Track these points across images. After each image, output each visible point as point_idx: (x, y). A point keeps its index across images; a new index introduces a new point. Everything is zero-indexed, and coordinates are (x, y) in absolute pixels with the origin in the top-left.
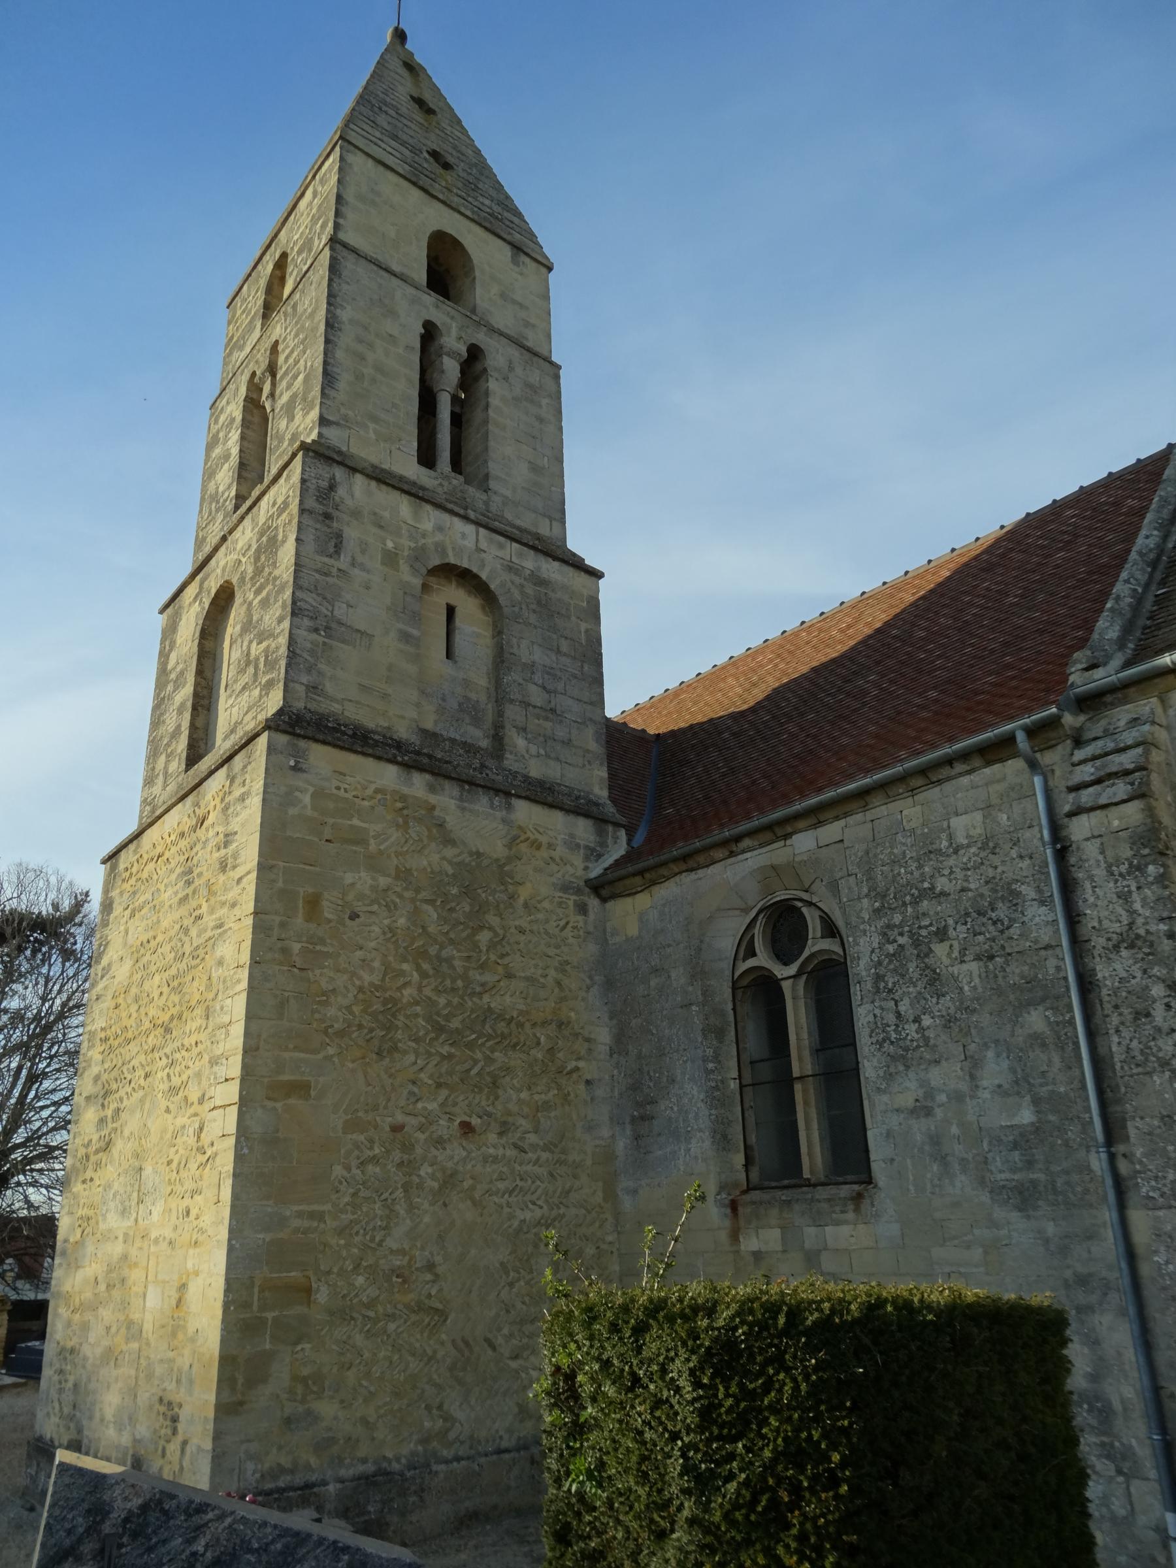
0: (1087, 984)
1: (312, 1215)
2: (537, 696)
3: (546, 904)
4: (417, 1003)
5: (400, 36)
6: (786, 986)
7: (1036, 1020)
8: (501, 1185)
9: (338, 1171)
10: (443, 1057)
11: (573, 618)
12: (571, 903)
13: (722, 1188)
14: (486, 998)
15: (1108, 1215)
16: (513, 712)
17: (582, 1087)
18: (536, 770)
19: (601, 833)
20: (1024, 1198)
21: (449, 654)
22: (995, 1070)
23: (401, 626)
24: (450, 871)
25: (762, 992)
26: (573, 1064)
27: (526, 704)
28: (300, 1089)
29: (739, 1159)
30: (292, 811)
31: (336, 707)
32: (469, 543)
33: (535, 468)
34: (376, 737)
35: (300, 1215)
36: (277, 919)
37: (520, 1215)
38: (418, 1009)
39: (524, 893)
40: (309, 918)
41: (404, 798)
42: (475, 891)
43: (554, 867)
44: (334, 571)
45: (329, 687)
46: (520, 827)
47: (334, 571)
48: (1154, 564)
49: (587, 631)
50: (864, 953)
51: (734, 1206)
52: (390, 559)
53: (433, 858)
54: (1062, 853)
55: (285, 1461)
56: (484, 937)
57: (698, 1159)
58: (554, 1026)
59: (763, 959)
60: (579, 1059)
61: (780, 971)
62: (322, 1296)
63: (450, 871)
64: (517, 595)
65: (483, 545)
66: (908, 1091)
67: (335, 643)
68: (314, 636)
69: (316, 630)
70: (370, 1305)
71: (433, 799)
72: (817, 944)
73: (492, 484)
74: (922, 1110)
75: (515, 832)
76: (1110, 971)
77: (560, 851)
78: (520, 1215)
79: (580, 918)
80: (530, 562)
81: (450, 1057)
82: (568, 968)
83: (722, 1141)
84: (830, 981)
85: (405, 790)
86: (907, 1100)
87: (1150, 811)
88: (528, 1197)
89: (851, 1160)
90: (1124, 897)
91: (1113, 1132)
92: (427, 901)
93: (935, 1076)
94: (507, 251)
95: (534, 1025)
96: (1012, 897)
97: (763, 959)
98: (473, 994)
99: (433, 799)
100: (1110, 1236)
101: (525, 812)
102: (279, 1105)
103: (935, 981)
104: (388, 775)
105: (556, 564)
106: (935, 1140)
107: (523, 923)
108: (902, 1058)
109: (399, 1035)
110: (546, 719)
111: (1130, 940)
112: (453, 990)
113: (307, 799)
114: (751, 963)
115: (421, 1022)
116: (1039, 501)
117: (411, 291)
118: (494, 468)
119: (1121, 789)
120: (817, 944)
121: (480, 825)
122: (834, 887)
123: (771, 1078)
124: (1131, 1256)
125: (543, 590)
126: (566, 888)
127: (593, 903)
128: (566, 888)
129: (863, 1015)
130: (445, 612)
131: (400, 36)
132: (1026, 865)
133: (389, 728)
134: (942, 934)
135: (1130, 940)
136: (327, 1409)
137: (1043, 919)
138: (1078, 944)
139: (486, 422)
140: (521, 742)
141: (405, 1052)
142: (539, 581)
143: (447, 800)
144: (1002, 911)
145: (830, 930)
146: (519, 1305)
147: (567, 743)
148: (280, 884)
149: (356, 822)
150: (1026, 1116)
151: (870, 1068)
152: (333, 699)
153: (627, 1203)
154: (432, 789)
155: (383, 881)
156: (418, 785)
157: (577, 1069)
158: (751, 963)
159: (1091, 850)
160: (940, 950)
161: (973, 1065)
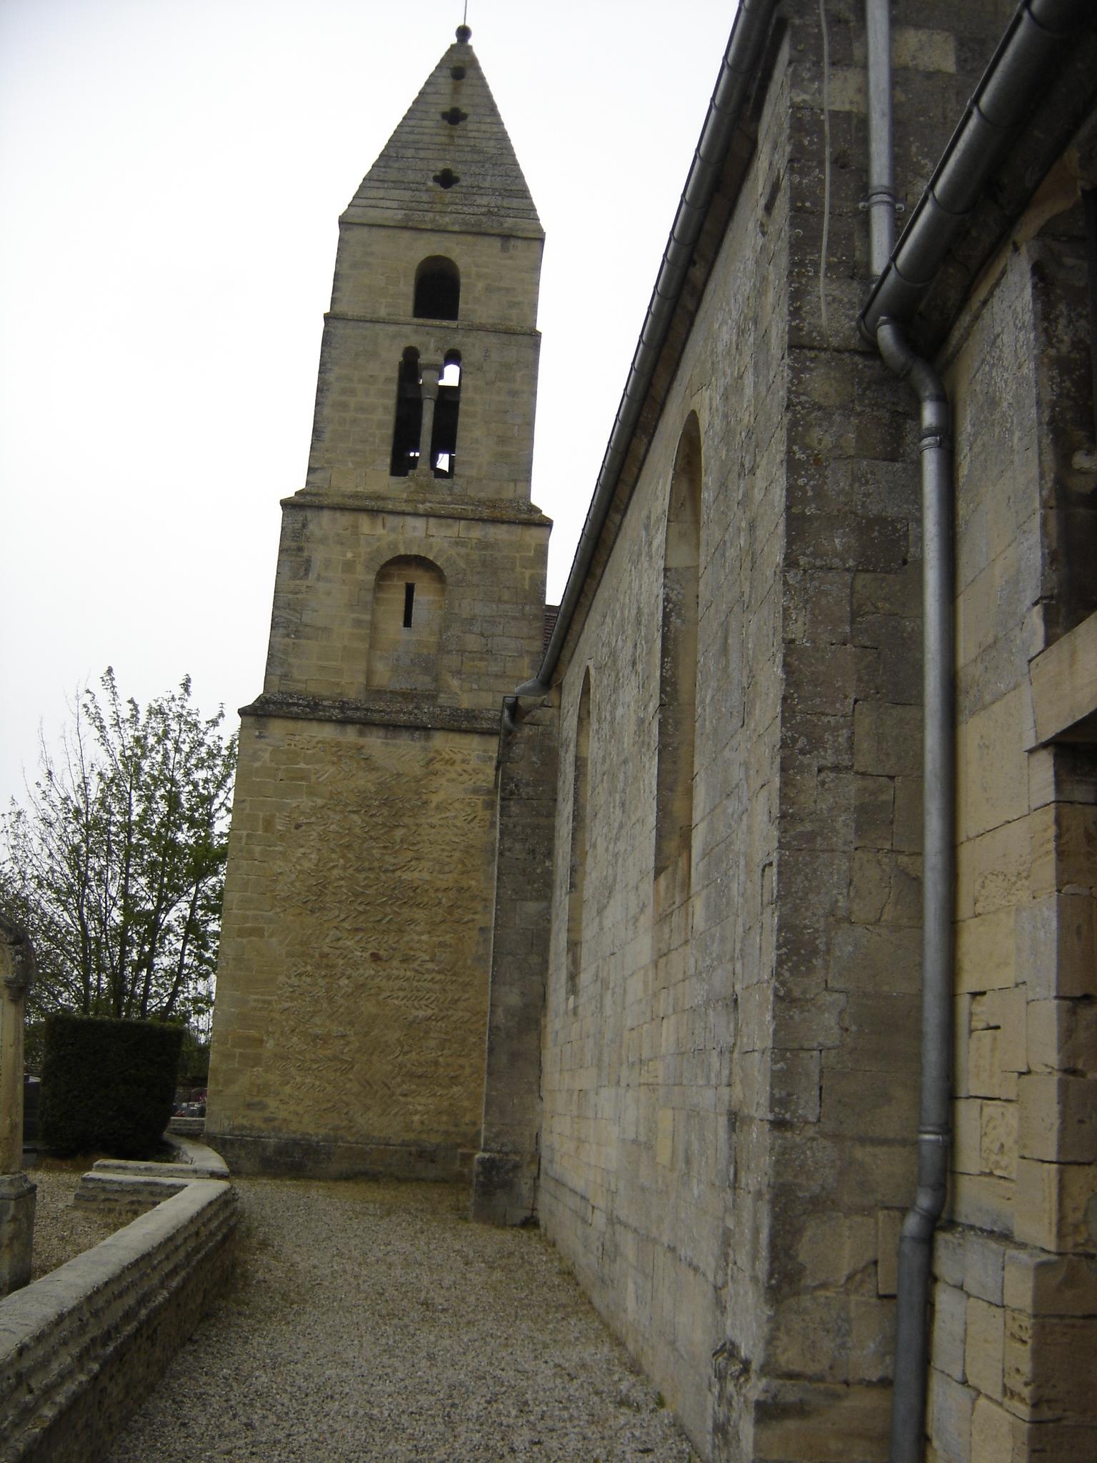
1: (264, 1002)
2: (473, 642)
3: (457, 805)
4: (342, 879)
5: (463, 33)
8: (401, 994)
9: (282, 978)
10: (361, 913)
11: (518, 569)
12: (480, 803)
14: (398, 873)
17: (476, 932)
18: (466, 702)
23: (355, 615)
24: (373, 789)
26: (471, 916)
27: (462, 652)
30: (257, 765)
31: (300, 686)
33: (502, 440)
34: (325, 703)
35: (255, 1000)
36: (245, 833)
37: (416, 1013)
38: (342, 883)
40: (266, 830)
41: (338, 744)
42: (392, 807)
43: (466, 777)
44: (304, 589)
45: (296, 674)
46: (437, 751)
47: (304, 589)
49: (531, 577)
53: (364, 781)
55: (245, 1122)
56: (399, 833)
58: (454, 891)
60: (475, 913)
62: (270, 1044)
63: (373, 789)
64: (462, 564)
65: (432, 531)
67: (303, 641)
68: (287, 640)
69: (288, 636)
70: (301, 1052)
71: (361, 741)
75: (432, 755)
78: (416, 1013)
79: (488, 813)
81: (365, 912)
82: (472, 851)
85: (341, 739)
88: (423, 1002)
92: (354, 812)
94: (497, 243)
95: (437, 890)
98: (386, 871)
99: (361, 741)
101: (440, 741)
102: (245, 941)
104: (328, 732)
105: (505, 527)
107: (434, 821)
109: (328, 899)
110: (481, 659)
112: (370, 869)
113: (267, 756)
115: (344, 890)
116: (516, 151)
125: (488, 553)
126: (476, 791)
128: (476, 791)
130: (404, 591)
131: (463, 33)
133: (340, 694)
136: (272, 1103)
140: (455, 683)
141: (331, 909)
143: (375, 743)
146: (409, 1065)
148: (247, 811)
149: (302, 765)
152: (299, 681)
154: (361, 734)
155: (320, 802)
156: (351, 735)
157: (473, 920)
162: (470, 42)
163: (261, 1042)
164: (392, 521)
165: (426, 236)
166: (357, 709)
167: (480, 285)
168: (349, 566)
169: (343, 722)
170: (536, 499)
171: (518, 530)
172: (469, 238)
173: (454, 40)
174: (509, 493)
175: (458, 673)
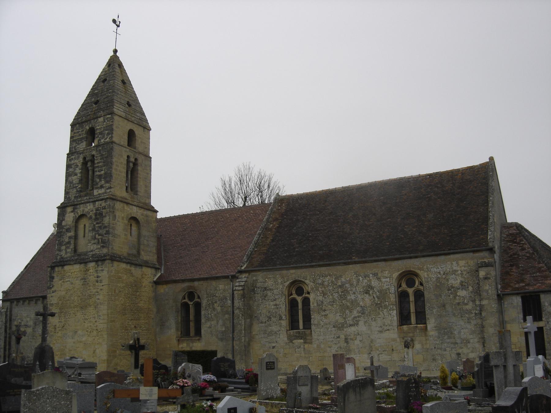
0: (233, 313)
5: (115, 51)
6: (191, 306)
7: (227, 316)
13: (177, 337)
15: (231, 342)
16: (142, 247)
19: (156, 271)
20: (222, 340)
21: (131, 235)
22: (221, 322)
25: (185, 306)
28: (114, 321)
29: (180, 333)
31: (115, 252)
32: (135, 211)
39: (144, 284)
42: (136, 286)
48: (256, 244)
50: (204, 303)
51: (179, 340)
52: (123, 218)
54: (233, 294)
56: (138, 293)
57: (172, 331)
59: (186, 300)
61: (189, 303)
62: (118, 352)
66: (208, 324)
72: (196, 300)
73: (138, 193)
74: (210, 327)
76: (236, 312)
77: (150, 275)
80: (146, 212)
83: (177, 330)
84: (198, 306)
86: (208, 326)
87: (244, 293)
89: (198, 332)
90: (239, 302)
91: (233, 332)
93: (212, 323)
94: (142, 129)
96: (226, 299)
97: (186, 300)
100: (231, 344)
101: (145, 269)
103: (214, 309)
104: (124, 266)
106: (211, 332)
108: (208, 319)
111: (239, 308)
114: (184, 301)
117: (125, 149)
118: (139, 189)
119: (241, 288)
120: (196, 300)
121: (137, 272)
122: (201, 291)
123: (186, 321)
124: (233, 347)
126: (150, 282)
127: (154, 285)
128: (150, 282)
129: (203, 313)
131: (115, 51)
132: (228, 295)
134: (216, 302)
135: (239, 308)
137: (229, 302)
138: (233, 306)
139: (137, 177)
142: (147, 216)
144: (224, 300)
145: (199, 297)
147: (150, 252)
150: (224, 329)
151: (203, 321)
153: (158, 339)
154: (131, 267)
156: (128, 267)
158: (184, 301)
159: (236, 295)
160: (215, 304)
161: (218, 322)
162: (117, 54)
163: (116, 351)
164: (131, 207)
165: (130, 122)
166: (497, 289)
167: (140, 141)
168: (123, 218)
169: (127, 263)
170: (153, 204)
171: (152, 212)
172: (137, 126)
173: (112, 54)
174: (147, 202)
175: (143, 250)
